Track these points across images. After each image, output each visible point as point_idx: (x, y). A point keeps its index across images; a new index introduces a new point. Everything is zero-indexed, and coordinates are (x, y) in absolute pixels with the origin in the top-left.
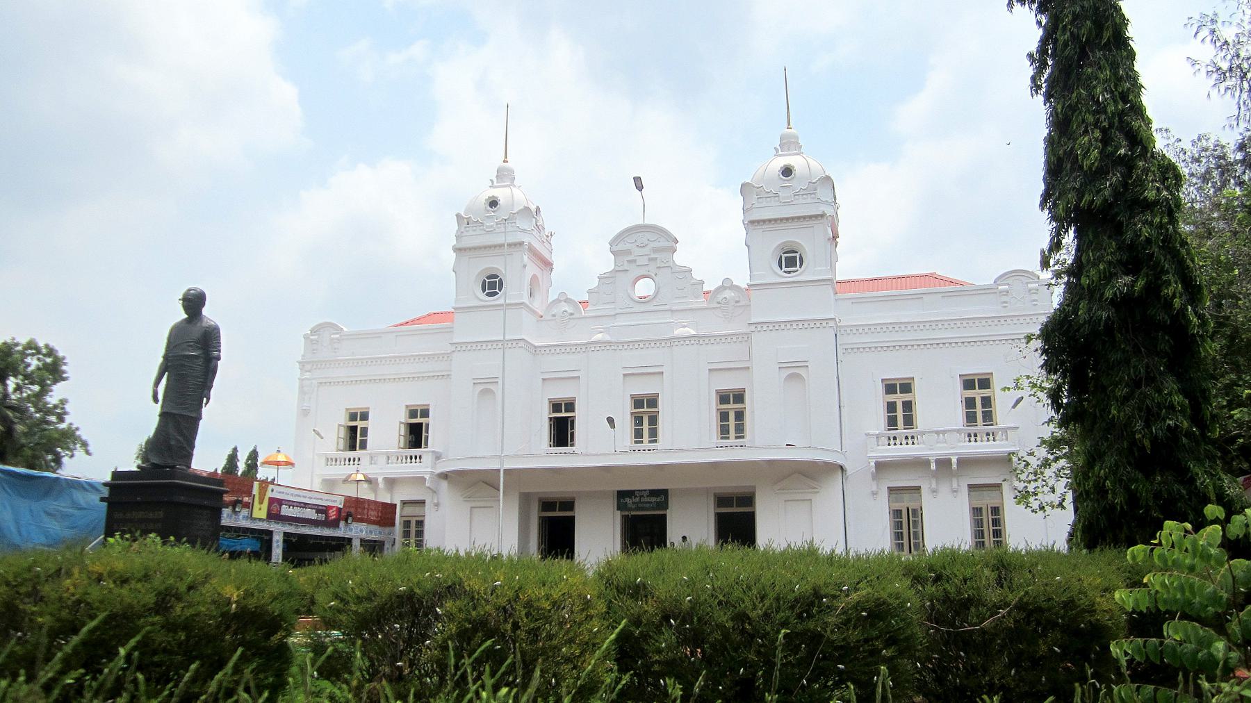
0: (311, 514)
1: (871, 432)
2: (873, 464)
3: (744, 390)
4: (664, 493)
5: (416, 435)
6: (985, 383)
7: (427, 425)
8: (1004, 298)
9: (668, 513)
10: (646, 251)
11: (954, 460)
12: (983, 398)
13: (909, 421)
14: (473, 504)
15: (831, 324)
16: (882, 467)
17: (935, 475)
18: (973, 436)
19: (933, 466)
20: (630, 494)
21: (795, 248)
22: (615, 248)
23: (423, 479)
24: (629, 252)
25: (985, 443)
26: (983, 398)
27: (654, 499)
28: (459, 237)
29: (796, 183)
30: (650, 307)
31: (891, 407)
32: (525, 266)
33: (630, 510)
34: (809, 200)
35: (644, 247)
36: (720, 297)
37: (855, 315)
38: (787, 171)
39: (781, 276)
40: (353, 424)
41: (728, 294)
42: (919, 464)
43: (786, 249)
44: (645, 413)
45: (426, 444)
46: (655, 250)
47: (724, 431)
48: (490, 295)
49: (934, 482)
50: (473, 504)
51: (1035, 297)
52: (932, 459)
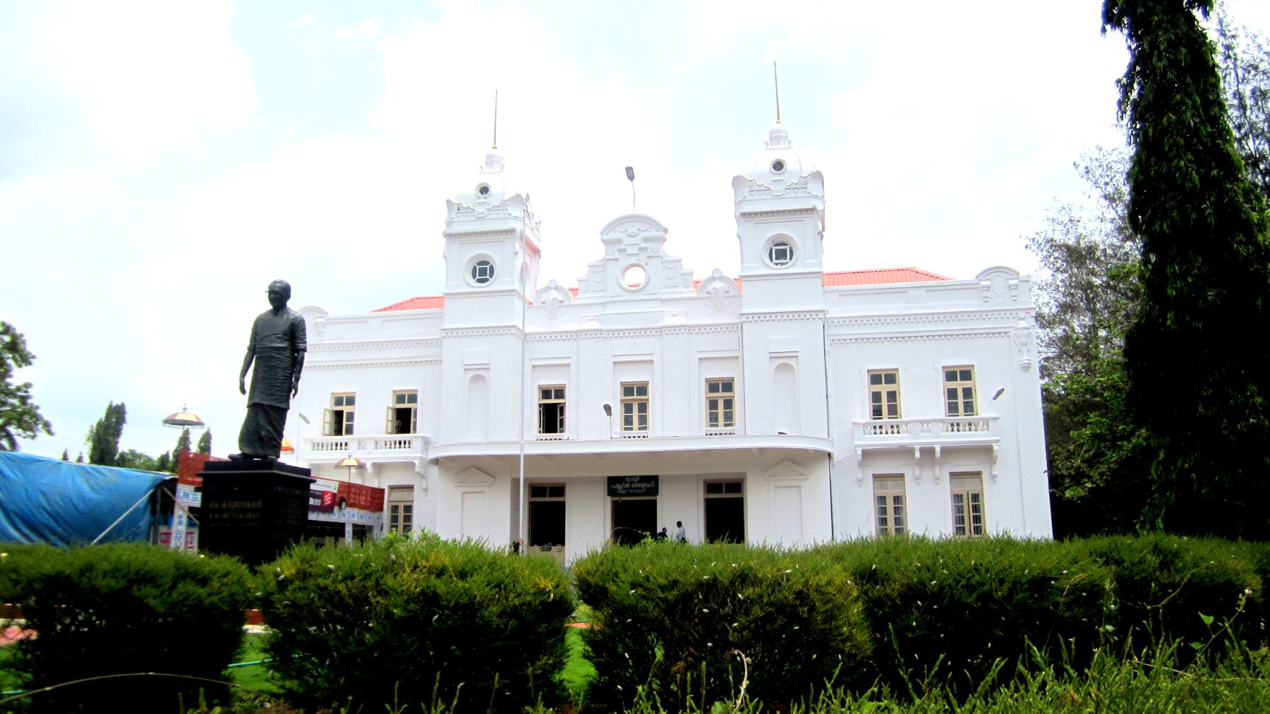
3: (733, 379)
4: (655, 479)
5: (403, 420)
8: (986, 294)
9: (659, 499)
11: (938, 449)
12: (964, 390)
13: (893, 411)
16: (869, 455)
17: (920, 463)
18: (955, 426)
19: (917, 455)
20: (621, 479)
21: (784, 241)
22: (606, 237)
23: (413, 465)
25: (968, 433)
26: (964, 390)
27: (644, 485)
28: (449, 223)
29: (788, 177)
30: (640, 296)
34: (800, 194)
35: (634, 238)
36: (710, 288)
37: (839, 310)
38: (778, 166)
39: (772, 268)
40: (339, 408)
41: (718, 285)
42: (904, 452)
44: (635, 400)
45: (415, 430)
46: (646, 240)
47: (713, 419)
48: (480, 281)
51: (1014, 293)
52: (917, 448)
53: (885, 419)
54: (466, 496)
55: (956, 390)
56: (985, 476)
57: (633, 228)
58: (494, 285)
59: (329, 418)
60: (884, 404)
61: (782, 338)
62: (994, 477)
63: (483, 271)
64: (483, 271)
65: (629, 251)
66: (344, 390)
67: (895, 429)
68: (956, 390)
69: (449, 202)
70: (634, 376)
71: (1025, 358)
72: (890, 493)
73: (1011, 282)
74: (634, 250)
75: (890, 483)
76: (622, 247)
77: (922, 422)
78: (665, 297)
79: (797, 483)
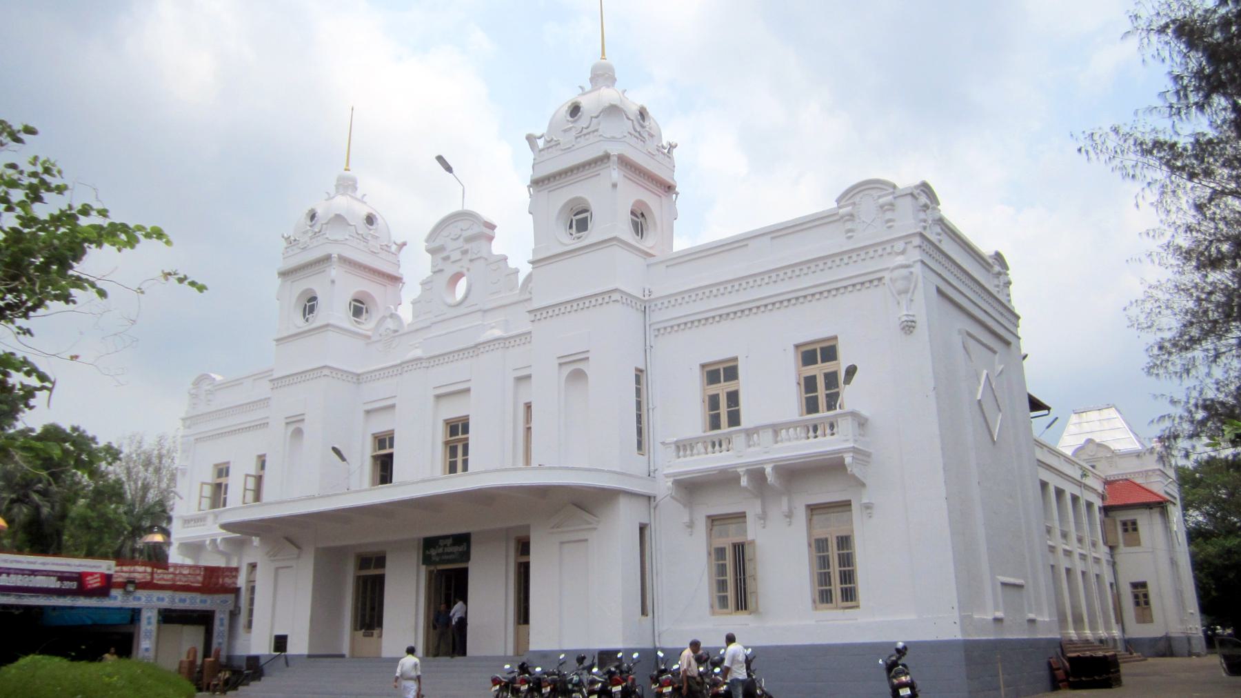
0: (53, 583)
1: (668, 440)
2: (670, 484)
7: (226, 486)
8: (849, 225)
10: (460, 243)
11: (768, 469)
12: (827, 376)
13: (734, 419)
18: (716, 444)
19: (744, 481)
24: (441, 249)
26: (827, 376)
31: (714, 402)
32: (615, 186)
33: (436, 563)
35: (463, 236)
40: (219, 481)
49: (758, 503)
51: (889, 215)
52: (741, 470)
54: (281, 571)
55: (814, 378)
59: (208, 491)
60: (724, 410)
62: (868, 507)
64: (579, 219)
65: (453, 259)
69: (531, 139)
70: (454, 410)
72: (726, 542)
73: (882, 201)
74: (456, 256)
75: (833, 517)
76: (444, 254)
77: (259, 479)
78: (487, 307)
79: (581, 536)
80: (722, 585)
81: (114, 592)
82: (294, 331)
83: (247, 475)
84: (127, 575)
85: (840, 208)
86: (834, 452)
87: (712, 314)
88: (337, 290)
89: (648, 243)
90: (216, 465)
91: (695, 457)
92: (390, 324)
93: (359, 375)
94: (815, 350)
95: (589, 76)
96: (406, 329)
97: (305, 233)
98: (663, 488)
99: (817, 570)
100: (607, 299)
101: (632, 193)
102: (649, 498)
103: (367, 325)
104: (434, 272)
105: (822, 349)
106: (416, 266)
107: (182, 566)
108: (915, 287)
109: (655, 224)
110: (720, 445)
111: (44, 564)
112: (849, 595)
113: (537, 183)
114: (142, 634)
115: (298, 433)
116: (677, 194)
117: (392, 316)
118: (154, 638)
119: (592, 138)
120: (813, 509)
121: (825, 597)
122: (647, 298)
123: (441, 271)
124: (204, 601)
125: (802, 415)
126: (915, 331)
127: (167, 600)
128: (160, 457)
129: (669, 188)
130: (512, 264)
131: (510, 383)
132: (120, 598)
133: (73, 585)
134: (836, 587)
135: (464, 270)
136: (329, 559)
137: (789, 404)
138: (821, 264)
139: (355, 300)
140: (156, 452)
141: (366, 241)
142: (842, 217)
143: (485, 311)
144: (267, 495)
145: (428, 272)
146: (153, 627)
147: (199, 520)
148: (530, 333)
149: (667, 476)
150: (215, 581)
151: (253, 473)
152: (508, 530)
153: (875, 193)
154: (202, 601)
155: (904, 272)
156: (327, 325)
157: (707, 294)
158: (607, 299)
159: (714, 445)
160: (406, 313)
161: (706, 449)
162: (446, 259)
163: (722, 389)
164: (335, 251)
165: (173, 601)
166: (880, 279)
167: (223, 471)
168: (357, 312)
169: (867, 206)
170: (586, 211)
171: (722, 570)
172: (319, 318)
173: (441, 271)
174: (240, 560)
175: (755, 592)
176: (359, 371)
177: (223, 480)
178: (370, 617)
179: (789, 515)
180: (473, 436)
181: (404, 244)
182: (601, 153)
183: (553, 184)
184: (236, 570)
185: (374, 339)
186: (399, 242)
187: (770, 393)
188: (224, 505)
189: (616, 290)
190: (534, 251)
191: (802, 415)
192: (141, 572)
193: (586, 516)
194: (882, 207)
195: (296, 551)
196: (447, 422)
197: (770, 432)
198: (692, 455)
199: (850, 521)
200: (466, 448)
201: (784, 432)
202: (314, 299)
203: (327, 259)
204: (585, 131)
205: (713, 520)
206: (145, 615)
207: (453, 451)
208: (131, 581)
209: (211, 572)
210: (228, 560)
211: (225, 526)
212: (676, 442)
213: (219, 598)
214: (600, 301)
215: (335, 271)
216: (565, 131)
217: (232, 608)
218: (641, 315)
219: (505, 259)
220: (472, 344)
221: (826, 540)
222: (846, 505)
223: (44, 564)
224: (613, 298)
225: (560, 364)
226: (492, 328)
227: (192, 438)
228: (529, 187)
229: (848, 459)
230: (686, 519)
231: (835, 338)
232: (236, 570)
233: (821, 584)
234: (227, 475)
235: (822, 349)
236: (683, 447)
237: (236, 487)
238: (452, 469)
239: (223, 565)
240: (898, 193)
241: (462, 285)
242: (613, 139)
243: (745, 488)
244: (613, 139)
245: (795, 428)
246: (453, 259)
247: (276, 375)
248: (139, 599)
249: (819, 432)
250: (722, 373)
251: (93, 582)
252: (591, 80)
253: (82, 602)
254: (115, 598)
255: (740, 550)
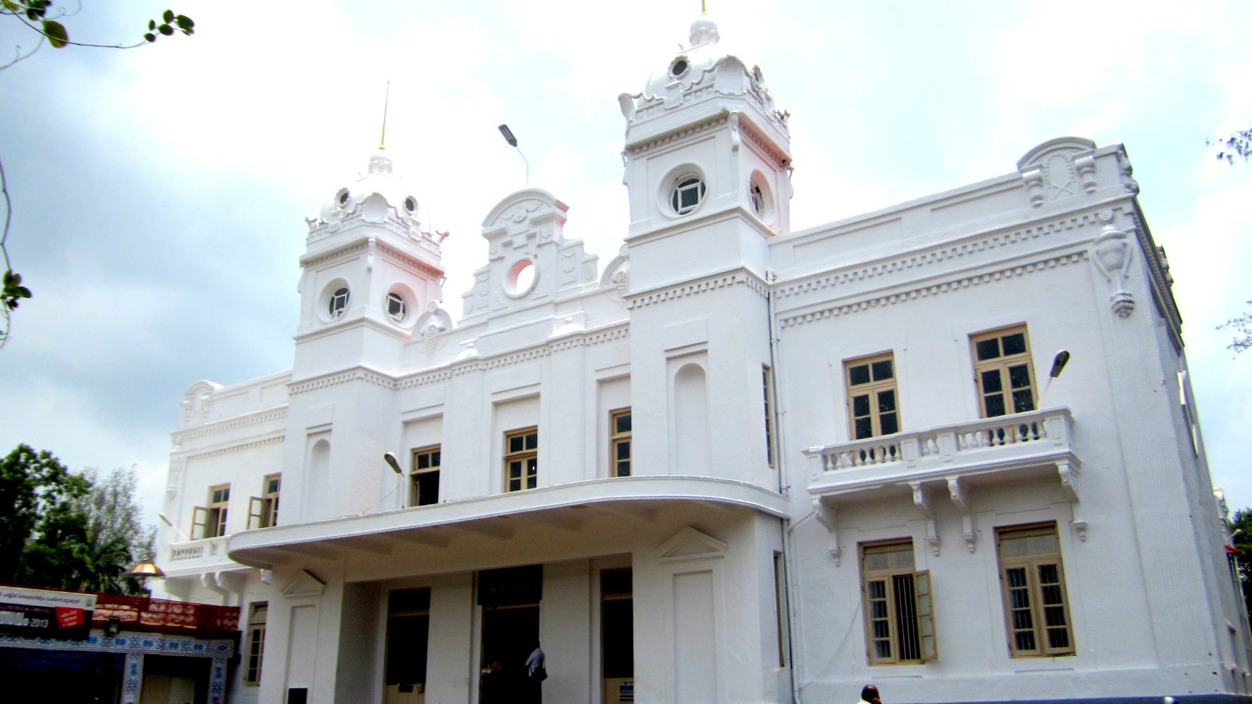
0: (20, 620)
1: (813, 448)
2: (816, 502)
6: (1015, 342)
7: (225, 511)
8: (1036, 192)
10: (525, 226)
11: (952, 482)
12: (1013, 371)
13: (890, 425)
14: (297, 602)
15: (740, 277)
16: (839, 508)
19: (918, 498)
24: (502, 233)
25: (1020, 444)
26: (1013, 371)
30: (528, 303)
31: (861, 405)
35: (527, 223)
40: (216, 505)
43: (683, 179)
44: (521, 453)
46: (535, 222)
49: (931, 525)
50: (297, 602)
51: (1089, 178)
52: (914, 484)
53: (877, 436)
54: (299, 611)
55: (866, 397)
56: (1062, 529)
57: (518, 211)
58: (705, 208)
61: (680, 323)
62: (1082, 528)
63: (688, 191)
64: (688, 191)
65: (516, 244)
66: (219, 480)
67: (1029, 430)
68: (866, 397)
69: (624, 100)
70: (517, 420)
71: (1118, 292)
72: (885, 575)
73: (1079, 162)
74: (521, 240)
76: (507, 239)
78: (559, 299)
79: (705, 566)
80: (881, 628)
81: (94, 634)
82: (317, 327)
83: (253, 498)
84: (109, 612)
85: (1022, 172)
86: (421, 578)
87: (858, 300)
88: (372, 284)
89: (768, 221)
90: (212, 488)
91: (840, 471)
92: (435, 322)
93: (396, 380)
94: (995, 341)
95: (689, 34)
96: (455, 326)
97: (336, 215)
98: (802, 505)
99: (871, 620)
100: (729, 281)
101: (749, 163)
102: (781, 520)
103: (406, 326)
104: (492, 261)
105: (1004, 339)
106: (464, 258)
107: (175, 604)
108: (1131, 260)
109: (772, 201)
110: (872, 456)
111: (10, 596)
112: (1061, 640)
113: (633, 150)
114: (125, 685)
115: (323, 447)
116: (791, 169)
117: (438, 312)
118: (138, 692)
119: (704, 95)
120: (1002, 533)
121: (1023, 642)
122: (770, 282)
123: (501, 258)
124: (198, 647)
125: (981, 417)
126: (1134, 313)
127: (155, 644)
128: (116, 495)
129: (783, 162)
130: (589, 250)
131: (593, 386)
132: (100, 640)
133: (44, 623)
134: (1041, 628)
135: (531, 257)
136: (361, 597)
137: (966, 405)
138: (1023, 232)
139: (392, 294)
140: (110, 489)
141: (407, 227)
142: (1027, 182)
143: (557, 304)
144: (285, 515)
145: (483, 260)
146: (138, 678)
147: (192, 552)
148: (627, 324)
149: (812, 492)
150: (213, 622)
151: (260, 495)
152: (591, 561)
153: (1069, 154)
154: (196, 647)
155: (1117, 243)
156: (362, 320)
157: (851, 276)
158: (729, 281)
159: (863, 456)
160: (456, 311)
161: (853, 461)
162: (508, 244)
163: (872, 389)
164: (373, 235)
165: (162, 647)
166: (1080, 254)
167: (221, 494)
168: (394, 308)
169: (1058, 169)
170: (696, 181)
171: (880, 609)
172: (351, 312)
173: (501, 258)
174: (241, 599)
175: (932, 636)
176: (396, 373)
177: (221, 505)
178: (408, 667)
179: (972, 541)
180: (543, 451)
181: (446, 235)
182: (718, 111)
183: (654, 151)
184: (237, 610)
185: (414, 339)
186: (442, 232)
187: (939, 393)
188: (222, 534)
189: (742, 269)
190: (631, 228)
191: (981, 417)
192: (126, 613)
193: (712, 543)
194: (1079, 168)
195: (319, 585)
196: (508, 434)
197: (915, 441)
198: (835, 468)
199: (1057, 548)
200: (533, 463)
201: (930, 442)
202: (344, 291)
203: (363, 244)
204: (695, 88)
205: (866, 548)
206: (130, 662)
207: (515, 469)
208: (114, 621)
209: (205, 613)
210: (226, 598)
211: (235, 555)
212: (824, 450)
213: (215, 644)
214: (712, 285)
215: (372, 259)
216: (669, 88)
217: (231, 656)
218: (765, 302)
219: (581, 244)
220: (543, 341)
221: (1023, 570)
222: (1049, 527)
223: (10, 596)
224: (738, 279)
225: (669, 359)
226: (567, 322)
227: (183, 456)
228: (625, 154)
229: (1063, 468)
230: (833, 546)
231: (1024, 325)
232: (237, 610)
233: (877, 635)
234: (226, 498)
235: (1004, 339)
236: (830, 457)
237: (239, 515)
238: (515, 486)
239: (220, 604)
240: (1097, 154)
241: (526, 277)
242: (731, 96)
243: (919, 507)
244: (731, 96)
245: (974, 433)
246: (516, 244)
247: (295, 379)
248: (123, 642)
249: (1006, 438)
250: (872, 372)
251: (70, 621)
252: (691, 39)
253: (54, 645)
254: (95, 640)
255: (906, 586)
